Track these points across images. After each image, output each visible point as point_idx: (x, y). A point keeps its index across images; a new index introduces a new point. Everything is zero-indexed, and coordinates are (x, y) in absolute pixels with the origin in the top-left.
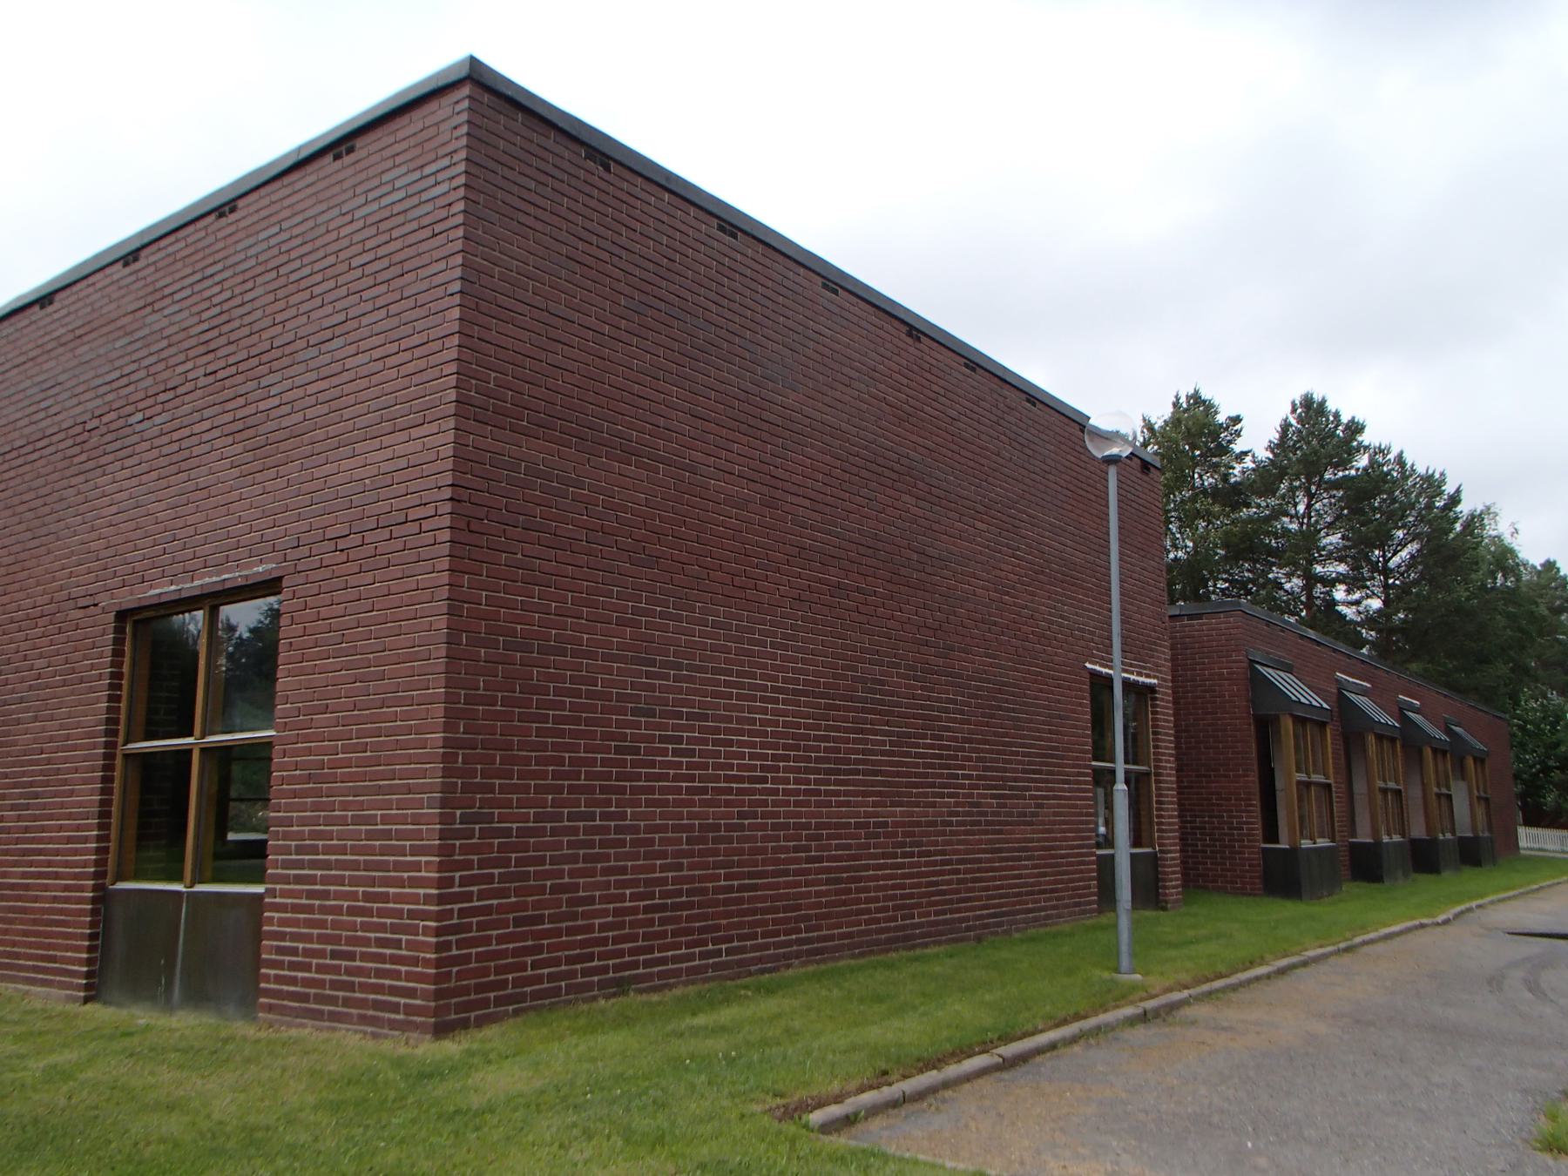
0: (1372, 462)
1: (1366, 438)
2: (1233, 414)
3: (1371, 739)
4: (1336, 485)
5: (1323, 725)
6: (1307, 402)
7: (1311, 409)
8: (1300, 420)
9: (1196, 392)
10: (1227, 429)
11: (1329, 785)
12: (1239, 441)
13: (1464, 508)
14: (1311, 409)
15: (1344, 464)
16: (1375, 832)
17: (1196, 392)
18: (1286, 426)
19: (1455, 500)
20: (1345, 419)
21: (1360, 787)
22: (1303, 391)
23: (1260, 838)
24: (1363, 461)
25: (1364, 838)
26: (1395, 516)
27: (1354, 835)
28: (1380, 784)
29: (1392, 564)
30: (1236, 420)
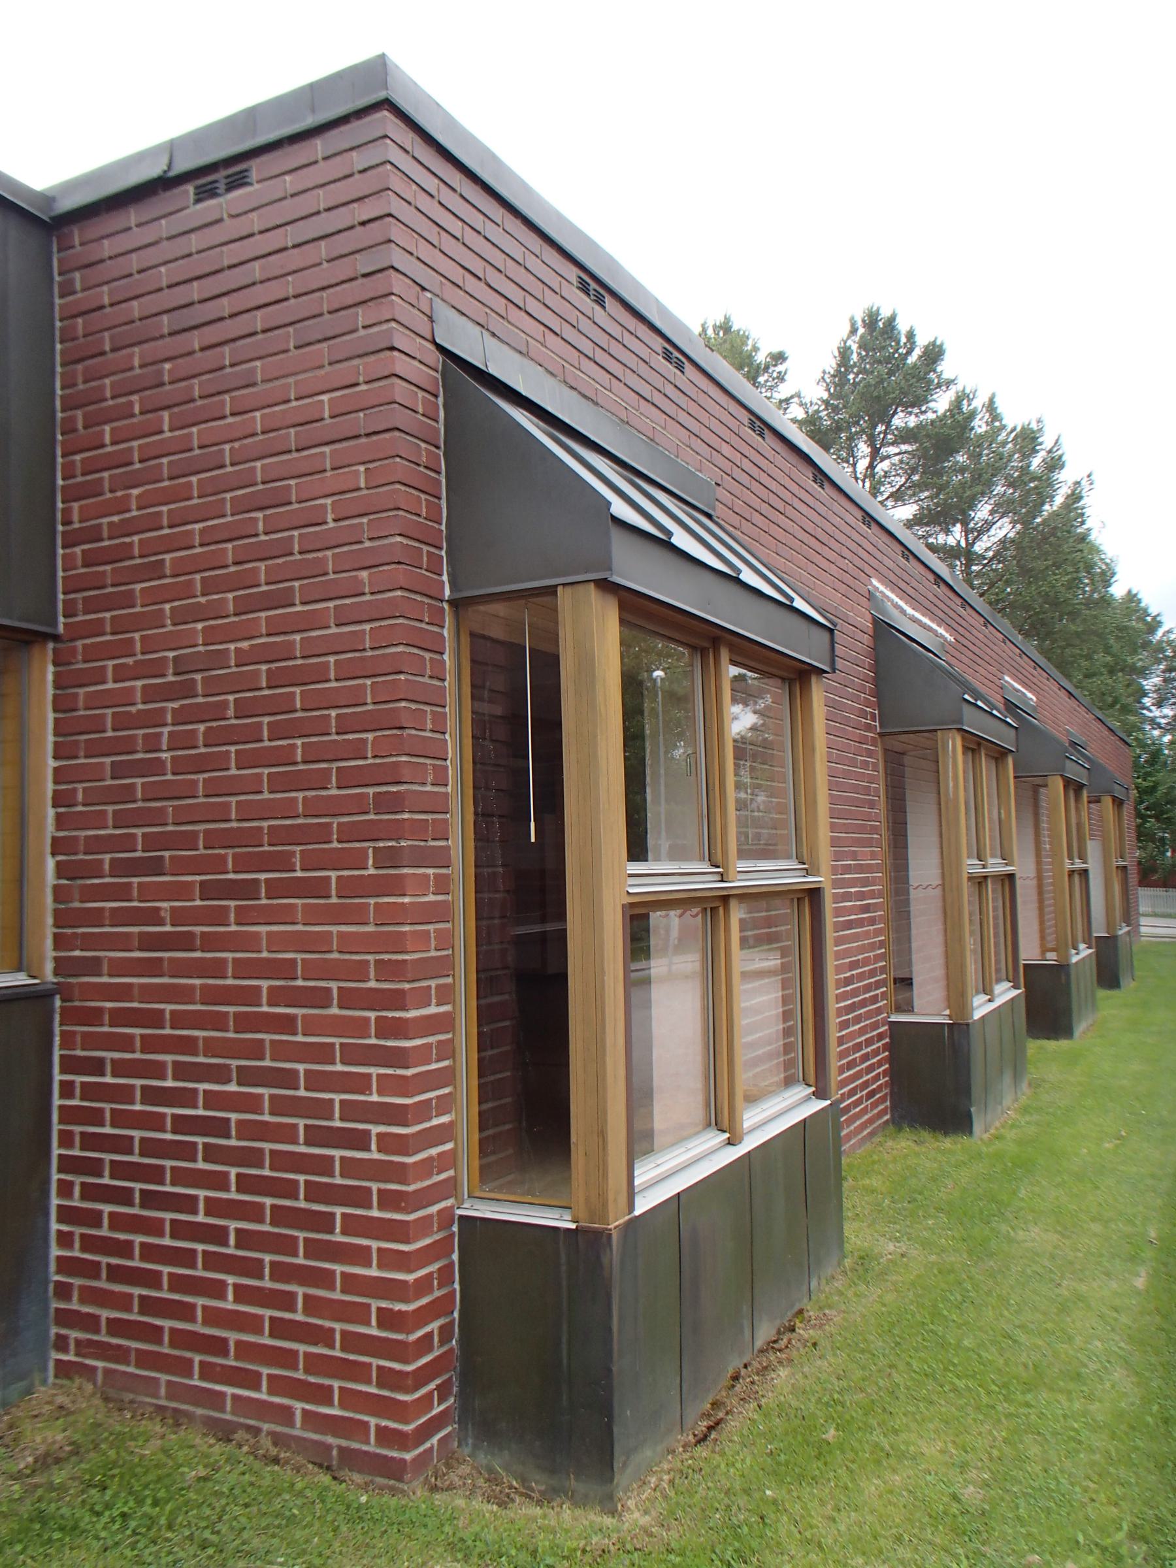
0: (957, 404)
1: (946, 368)
2: (776, 350)
3: (954, 744)
4: (906, 435)
5: (797, 677)
6: (871, 319)
7: (878, 332)
8: (863, 345)
9: (727, 320)
10: (767, 368)
11: (814, 895)
12: (782, 387)
13: (1066, 478)
14: (878, 332)
15: (919, 402)
16: (957, 998)
17: (727, 320)
18: (844, 353)
19: (1054, 464)
20: (922, 341)
21: (924, 868)
22: (866, 305)
23: (466, 1170)
24: (941, 403)
25: (929, 1007)
26: (981, 481)
27: (907, 1006)
28: (972, 866)
29: (978, 548)
30: (780, 357)
